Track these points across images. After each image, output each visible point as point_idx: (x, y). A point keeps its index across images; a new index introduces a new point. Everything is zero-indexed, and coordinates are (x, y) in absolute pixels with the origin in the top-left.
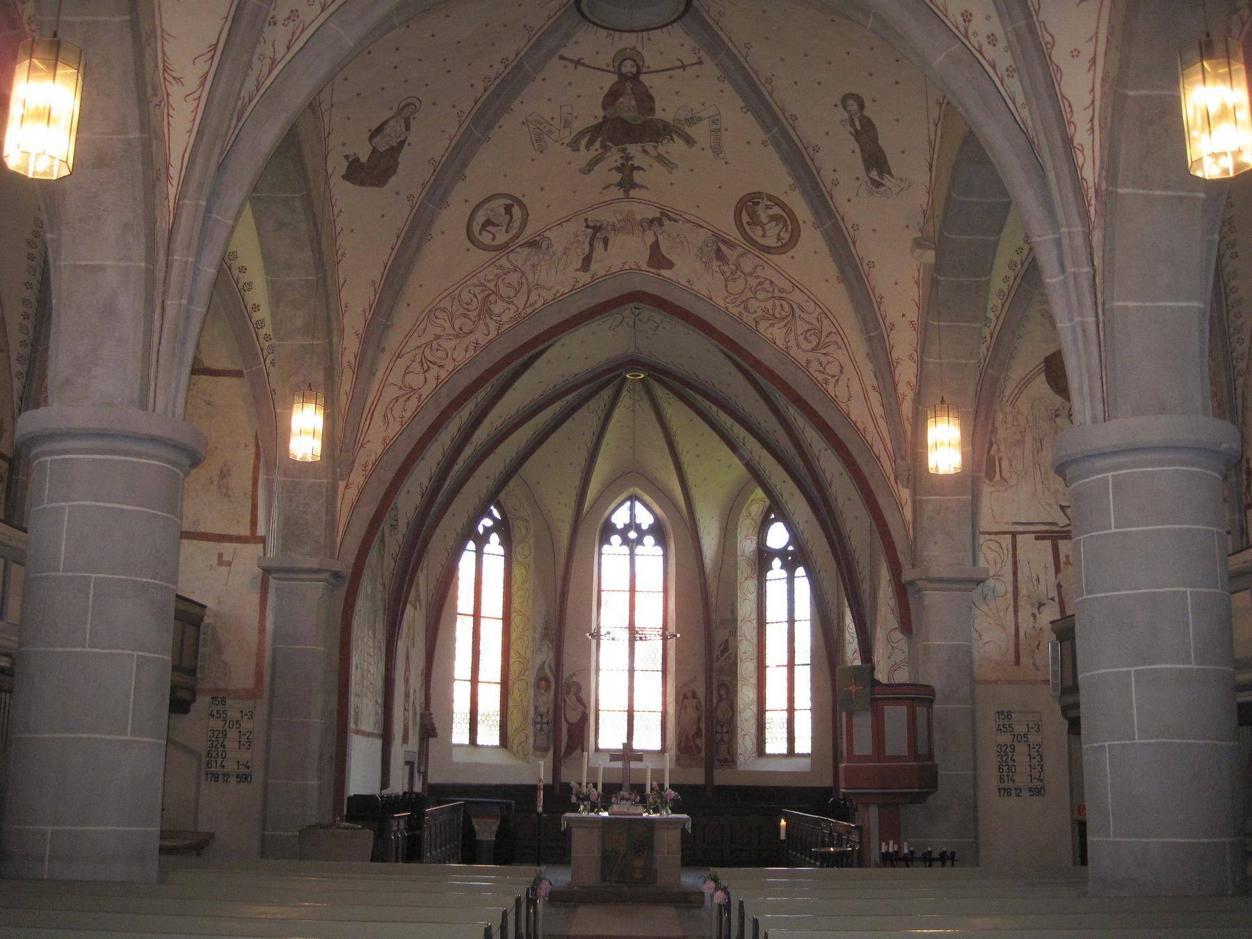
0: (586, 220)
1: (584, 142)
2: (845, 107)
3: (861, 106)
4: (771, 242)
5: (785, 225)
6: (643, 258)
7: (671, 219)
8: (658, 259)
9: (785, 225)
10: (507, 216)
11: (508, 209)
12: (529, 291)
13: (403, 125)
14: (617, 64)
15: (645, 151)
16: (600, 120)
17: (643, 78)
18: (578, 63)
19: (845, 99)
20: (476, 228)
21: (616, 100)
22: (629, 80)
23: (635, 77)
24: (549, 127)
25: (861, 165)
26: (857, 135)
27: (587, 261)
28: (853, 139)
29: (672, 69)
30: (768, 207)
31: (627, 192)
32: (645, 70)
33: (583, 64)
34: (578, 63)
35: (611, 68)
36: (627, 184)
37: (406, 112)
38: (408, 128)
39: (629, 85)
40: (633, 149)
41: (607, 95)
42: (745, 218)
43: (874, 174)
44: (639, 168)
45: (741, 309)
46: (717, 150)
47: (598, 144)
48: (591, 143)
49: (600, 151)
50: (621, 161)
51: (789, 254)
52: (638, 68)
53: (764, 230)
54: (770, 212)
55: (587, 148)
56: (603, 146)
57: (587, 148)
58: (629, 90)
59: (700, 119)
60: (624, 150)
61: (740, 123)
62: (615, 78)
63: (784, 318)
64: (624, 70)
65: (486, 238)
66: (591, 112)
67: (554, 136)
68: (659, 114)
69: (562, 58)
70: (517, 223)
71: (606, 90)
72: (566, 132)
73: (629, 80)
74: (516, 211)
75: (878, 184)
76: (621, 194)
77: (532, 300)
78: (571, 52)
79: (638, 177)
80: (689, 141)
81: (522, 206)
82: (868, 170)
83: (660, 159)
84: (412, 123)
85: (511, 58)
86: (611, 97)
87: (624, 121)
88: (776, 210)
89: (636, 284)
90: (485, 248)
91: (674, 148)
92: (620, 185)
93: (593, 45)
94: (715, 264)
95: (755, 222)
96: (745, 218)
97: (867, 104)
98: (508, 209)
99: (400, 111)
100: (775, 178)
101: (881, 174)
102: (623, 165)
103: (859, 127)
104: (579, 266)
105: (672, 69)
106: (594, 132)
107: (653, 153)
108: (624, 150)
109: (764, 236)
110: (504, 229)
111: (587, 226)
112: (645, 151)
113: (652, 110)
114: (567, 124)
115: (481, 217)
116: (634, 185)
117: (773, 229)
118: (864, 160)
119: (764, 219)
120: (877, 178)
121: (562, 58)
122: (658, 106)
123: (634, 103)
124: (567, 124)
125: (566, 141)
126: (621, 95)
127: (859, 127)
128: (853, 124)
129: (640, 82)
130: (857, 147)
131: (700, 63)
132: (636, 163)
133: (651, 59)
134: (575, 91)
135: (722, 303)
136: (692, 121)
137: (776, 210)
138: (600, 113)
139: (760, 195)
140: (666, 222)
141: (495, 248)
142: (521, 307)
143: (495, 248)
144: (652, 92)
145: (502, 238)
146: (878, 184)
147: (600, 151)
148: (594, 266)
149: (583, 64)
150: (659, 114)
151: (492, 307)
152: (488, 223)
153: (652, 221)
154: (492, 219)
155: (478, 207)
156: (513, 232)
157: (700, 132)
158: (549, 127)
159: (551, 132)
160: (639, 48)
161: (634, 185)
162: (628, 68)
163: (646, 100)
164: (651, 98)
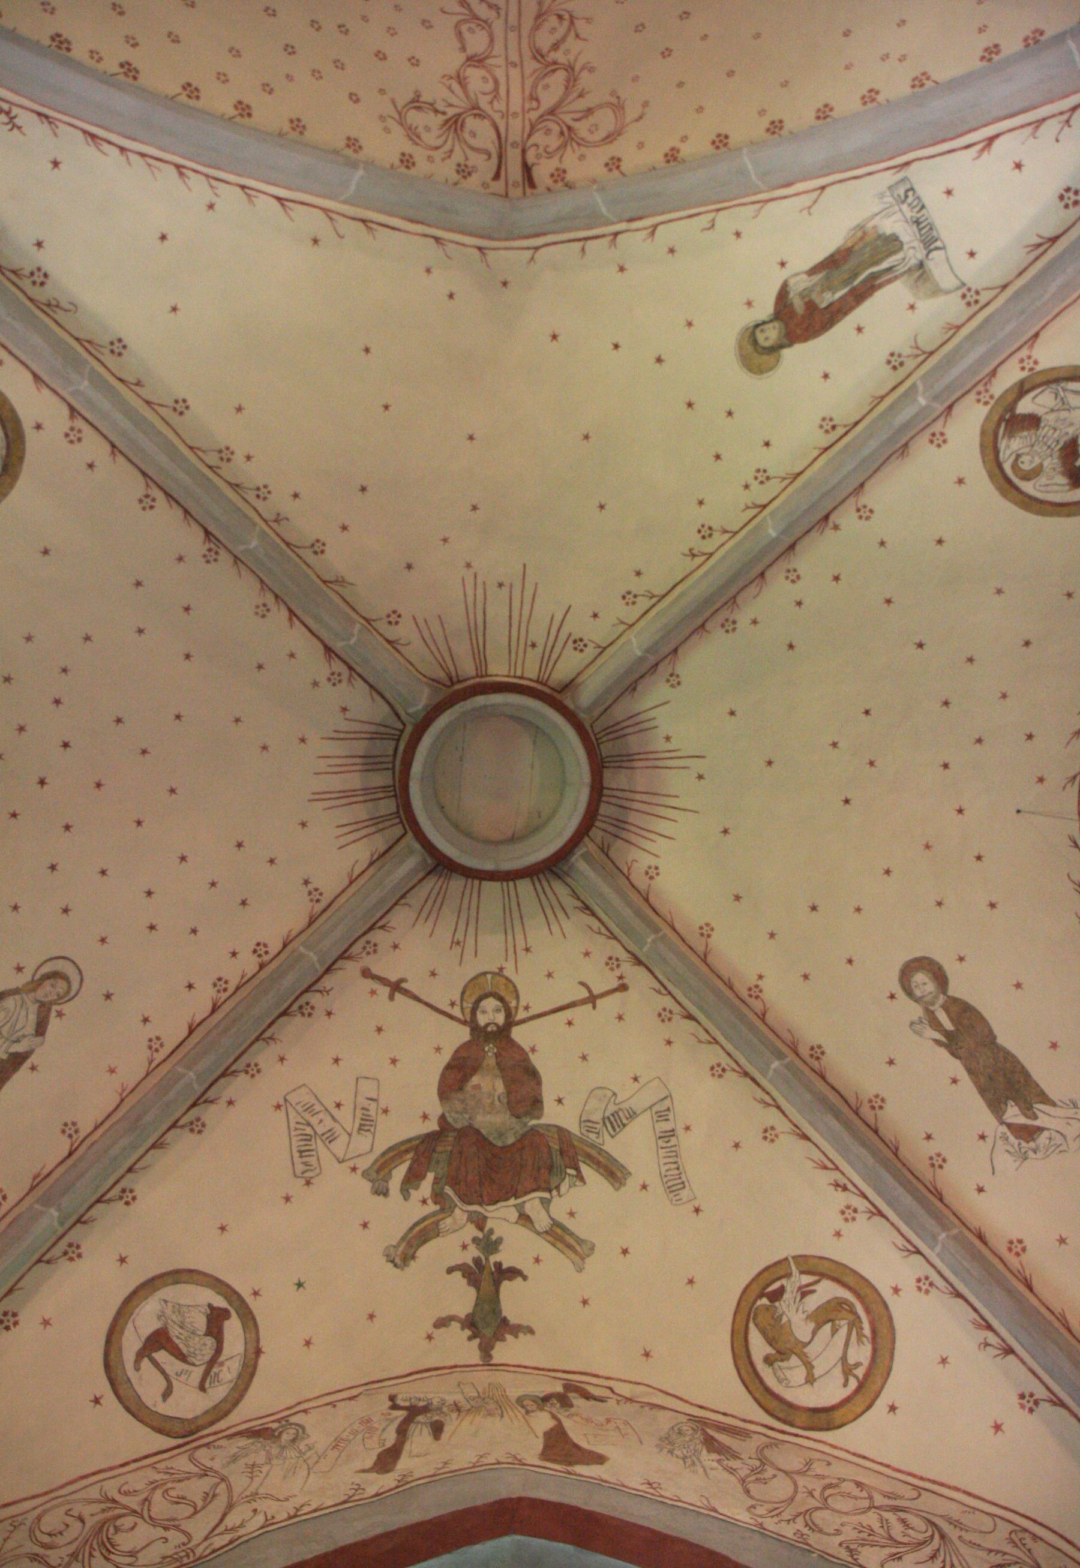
0: (392, 1398)
1: (399, 1173)
2: (909, 993)
3: (941, 978)
4: (830, 1391)
5: (855, 1323)
6: (531, 1449)
7: (588, 1396)
8: (559, 1447)
9: (855, 1323)
10: (210, 1341)
11: (216, 1319)
12: (230, 1506)
13: (33, 1018)
14: (468, 1006)
15: (524, 1219)
16: (433, 1126)
17: (518, 1034)
18: (396, 987)
19: (907, 971)
20: (131, 1343)
21: (465, 1079)
22: (491, 1050)
23: (502, 1034)
24: (329, 1123)
25: (978, 1102)
26: (951, 1043)
27: (387, 1460)
28: (943, 1053)
29: (572, 1005)
30: (805, 1292)
31: (486, 1351)
32: (521, 1015)
33: (407, 993)
34: (396, 987)
35: (456, 1012)
36: (488, 1325)
37: (47, 991)
38: (41, 1029)
39: (490, 1049)
40: (501, 1216)
41: (448, 1067)
42: (759, 1347)
43: (1013, 1114)
44: (514, 1273)
45: (800, 1524)
46: (675, 1184)
47: (426, 1187)
48: (413, 1178)
49: (432, 1207)
50: (473, 1252)
51: (881, 1404)
52: (509, 1014)
53: (809, 1366)
54: (812, 1302)
55: (405, 1193)
56: (438, 1196)
57: (405, 1193)
58: (490, 1060)
59: (632, 1115)
60: (480, 1222)
61: (711, 1102)
62: (463, 1034)
63: (922, 1544)
64: (482, 1020)
65: (147, 1383)
66: (413, 1106)
67: (338, 1146)
68: (553, 1115)
69: (366, 973)
70: (229, 1371)
71: (446, 1057)
72: (362, 1143)
73: (491, 1050)
74: (233, 1328)
75: (1028, 1133)
76: (470, 1352)
77: (231, 1520)
78: (388, 966)
79: (513, 1300)
80: (614, 1173)
81: (248, 1318)
82: (996, 1106)
83: (559, 1235)
84: (54, 1023)
85: (273, 951)
86: (457, 1074)
87: (482, 1141)
88: (827, 1291)
89: (510, 1486)
90: (136, 1409)
91: (583, 1200)
92: (470, 1323)
93: (425, 951)
94: (709, 1459)
95: (783, 1349)
96: (759, 1347)
97: (951, 968)
98: (216, 1319)
99: (36, 984)
100: (809, 1208)
101: (1027, 1109)
102: (477, 1261)
103: (949, 1026)
104: (369, 1463)
105: (572, 1005)
106: (421, 1152)
107: (542, 1221)
108: (480, 1222)
109: (810, 1380)
110: (197, 1373)
111: (395, 1407)
112: (524, 1219)
113: (536, 1104)
114: (366, 1125)
115: (146, 1319)
116: (504, 1328)
117: (827, 1349)
118: (982, 1091)
119: (802, 1330)
120: (1022, 1120)
121: (366, 973)
122: (547, 161)
123: (500, 1088)
124: (366, 1125)
125: (364, 1163)
126: (475, 1070)
127: (949, 1026)
128: (935, 1024)
129: (513, 1044)
130: (956, 1067)
131: (623, 988)
132: (505, 1257)
133: (534, 994)
134: (382, 1059)
135: (744, 1517)
136: (616, 1122)
137: (827, 1291)
138: (435, 1108)
139: (778, 1269)
140: (577, 1401)
141: (161, 1425)
142: (197, 1538)
143: (161, 1425)
144: (536, 1060)
145: (188, 1403)
146: (1028, 1133)
147: (432, 1207)
148: (404, 1463)
149: (407, 993)
150: (553, 1115)
151: (118, 1539)
152: (159, 1340)
153: (546, 1399)
154: (174, 1332)
155: (150, 1285)
156: (218, 1393)
157: (634, 1146)
158: (329, 1123)
159: (330, 1137)
160: (509, 972)
161: (504, 1328)
162: (490, 1014)
163: (523, 1082)
164: (533, 1074)
